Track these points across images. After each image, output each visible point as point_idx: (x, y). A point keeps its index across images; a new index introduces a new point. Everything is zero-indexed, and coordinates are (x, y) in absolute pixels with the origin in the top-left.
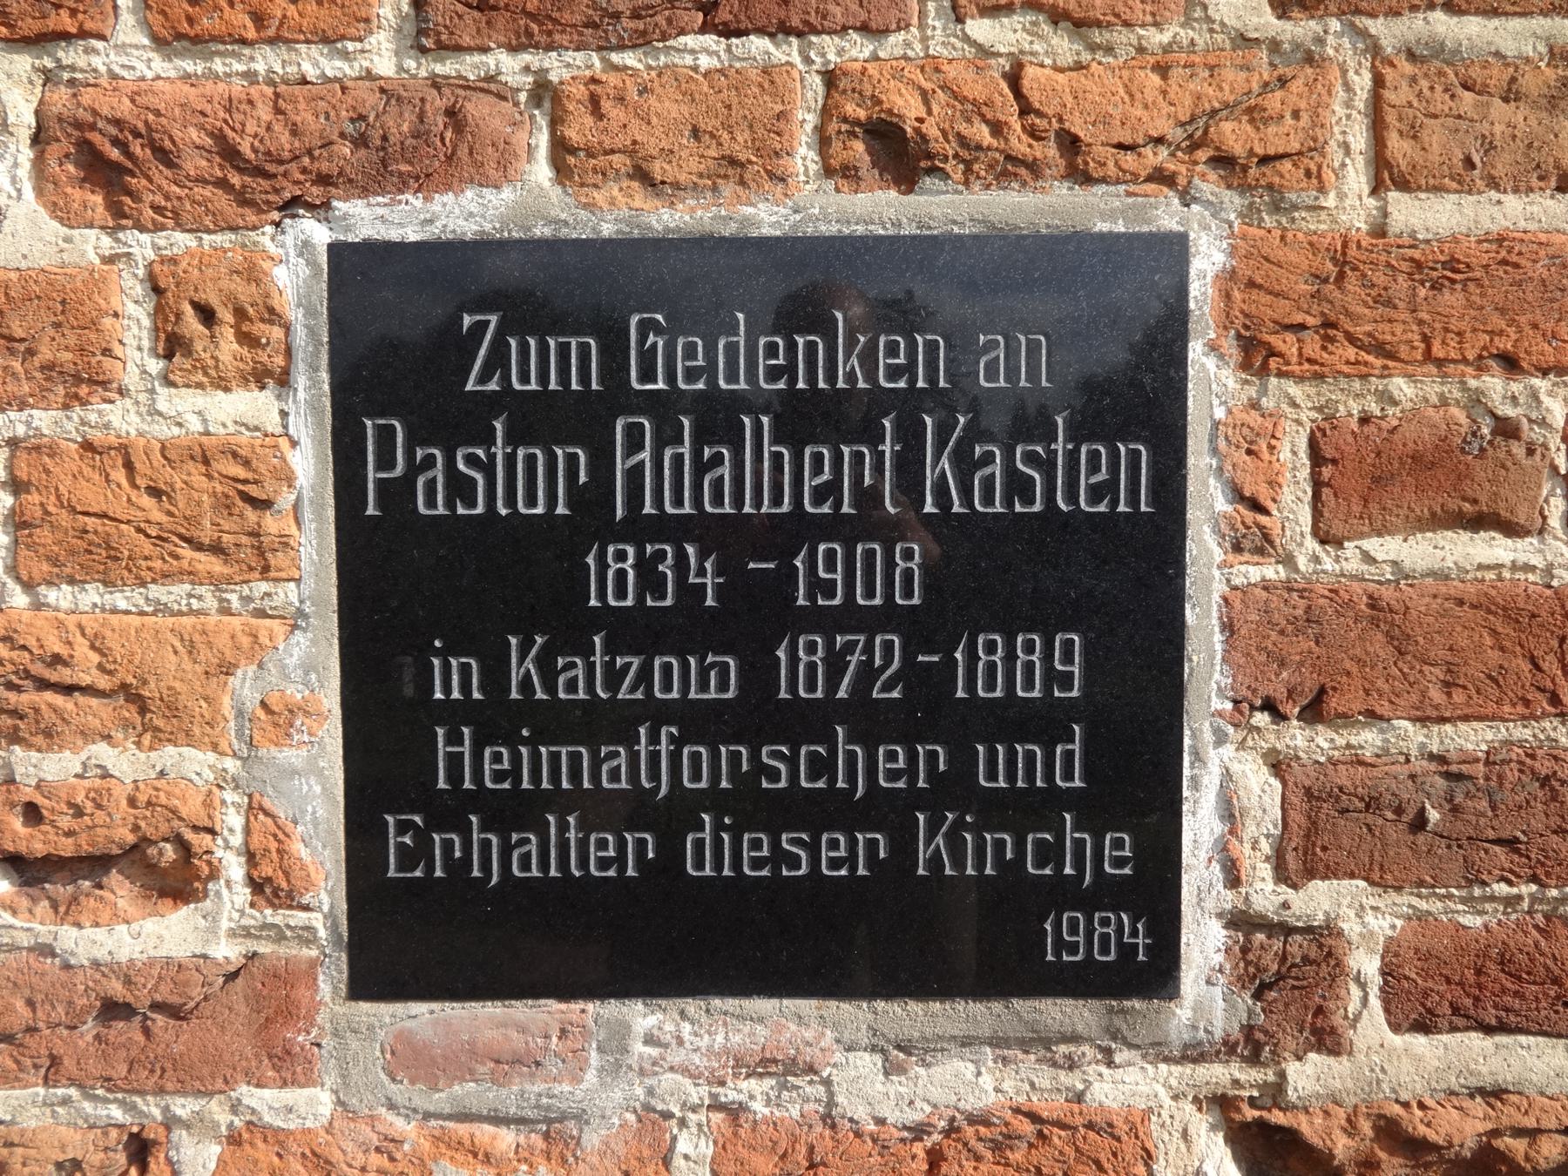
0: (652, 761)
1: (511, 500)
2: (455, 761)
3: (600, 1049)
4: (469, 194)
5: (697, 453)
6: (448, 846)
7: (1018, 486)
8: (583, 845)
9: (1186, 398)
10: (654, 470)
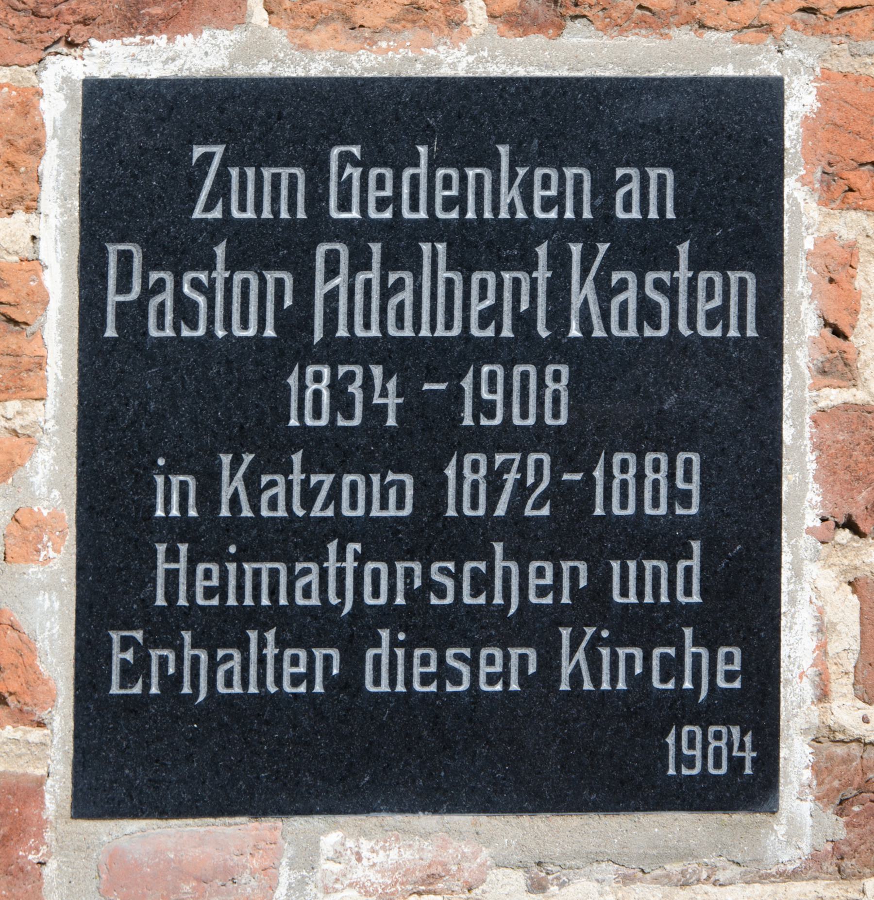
0: (341, 578)
1: (228, 325)
2: (172, 576)
3: (292, 867)
4: (206, 34)
5: (384, 279)
6: (163, 662)
7: (648, 312)
8: (278, 659)
9: (782, 230)
10: (350, 296)
